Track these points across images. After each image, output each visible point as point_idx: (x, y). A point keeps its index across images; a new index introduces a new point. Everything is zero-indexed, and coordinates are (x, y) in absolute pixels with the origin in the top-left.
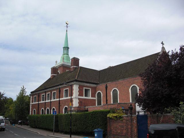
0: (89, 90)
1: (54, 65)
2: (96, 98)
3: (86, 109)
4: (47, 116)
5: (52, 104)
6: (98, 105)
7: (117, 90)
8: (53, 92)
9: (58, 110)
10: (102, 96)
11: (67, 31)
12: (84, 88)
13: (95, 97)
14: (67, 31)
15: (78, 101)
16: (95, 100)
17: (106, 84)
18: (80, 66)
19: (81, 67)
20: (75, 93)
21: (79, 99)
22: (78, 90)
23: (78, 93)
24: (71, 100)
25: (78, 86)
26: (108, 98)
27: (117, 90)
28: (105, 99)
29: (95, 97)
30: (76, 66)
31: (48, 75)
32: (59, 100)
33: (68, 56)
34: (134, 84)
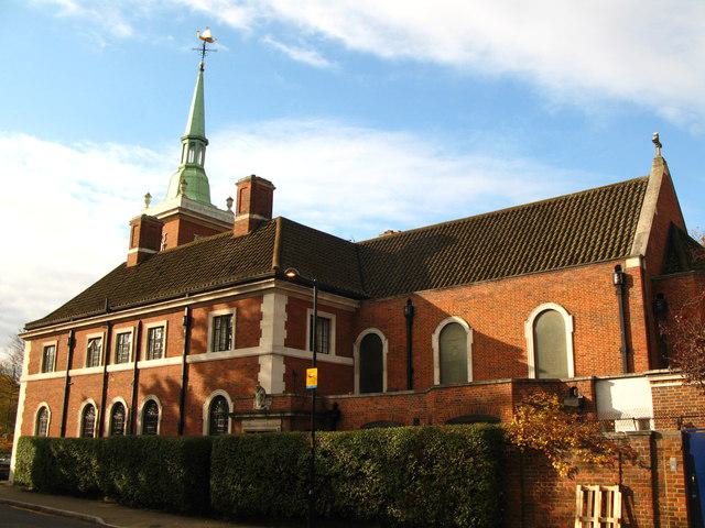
0: (329, 320)
1: (138, 210)
2: (354, 360)
3: (331, 409)
4: (685, 486)
5: (111, 379)
6: (364, 389)
7: (383, 337)
8: (148, 325)
9: (69, 412)
10: (385, 350)
11: (202, 70)
12: (310, 312)
13: (351, 356)
14: (202, 70)
15: (282, 368)
16: (353, 367)
17: (409, 302)
18: (276, 213)
19: (284, 221)
20: (639, 281)
21: (288, 360)
22: (284, 317)
23: (284, 334)
24: (252, 365)
25: (284, 300)
26: (417, 359)
27: (383, 337)
28: (403, 368)
29: (351, 356)
30: (261, 214)
31: (118, 251)
32: (106, 375)
33: (201, 174)
34: (369, 327)
